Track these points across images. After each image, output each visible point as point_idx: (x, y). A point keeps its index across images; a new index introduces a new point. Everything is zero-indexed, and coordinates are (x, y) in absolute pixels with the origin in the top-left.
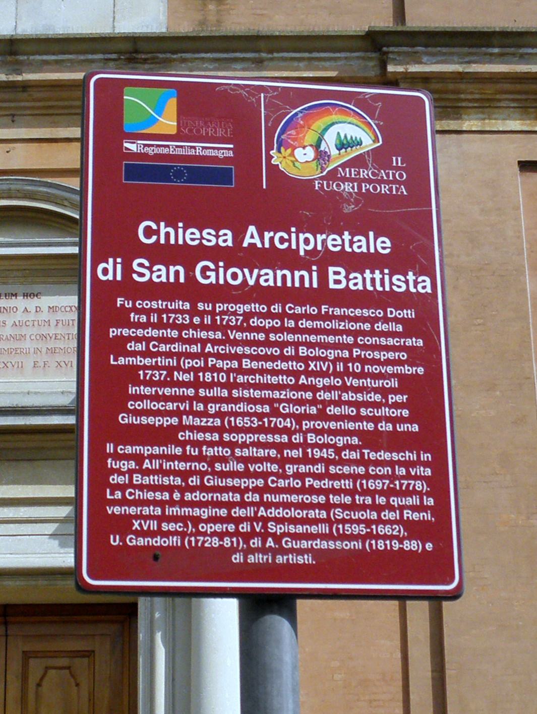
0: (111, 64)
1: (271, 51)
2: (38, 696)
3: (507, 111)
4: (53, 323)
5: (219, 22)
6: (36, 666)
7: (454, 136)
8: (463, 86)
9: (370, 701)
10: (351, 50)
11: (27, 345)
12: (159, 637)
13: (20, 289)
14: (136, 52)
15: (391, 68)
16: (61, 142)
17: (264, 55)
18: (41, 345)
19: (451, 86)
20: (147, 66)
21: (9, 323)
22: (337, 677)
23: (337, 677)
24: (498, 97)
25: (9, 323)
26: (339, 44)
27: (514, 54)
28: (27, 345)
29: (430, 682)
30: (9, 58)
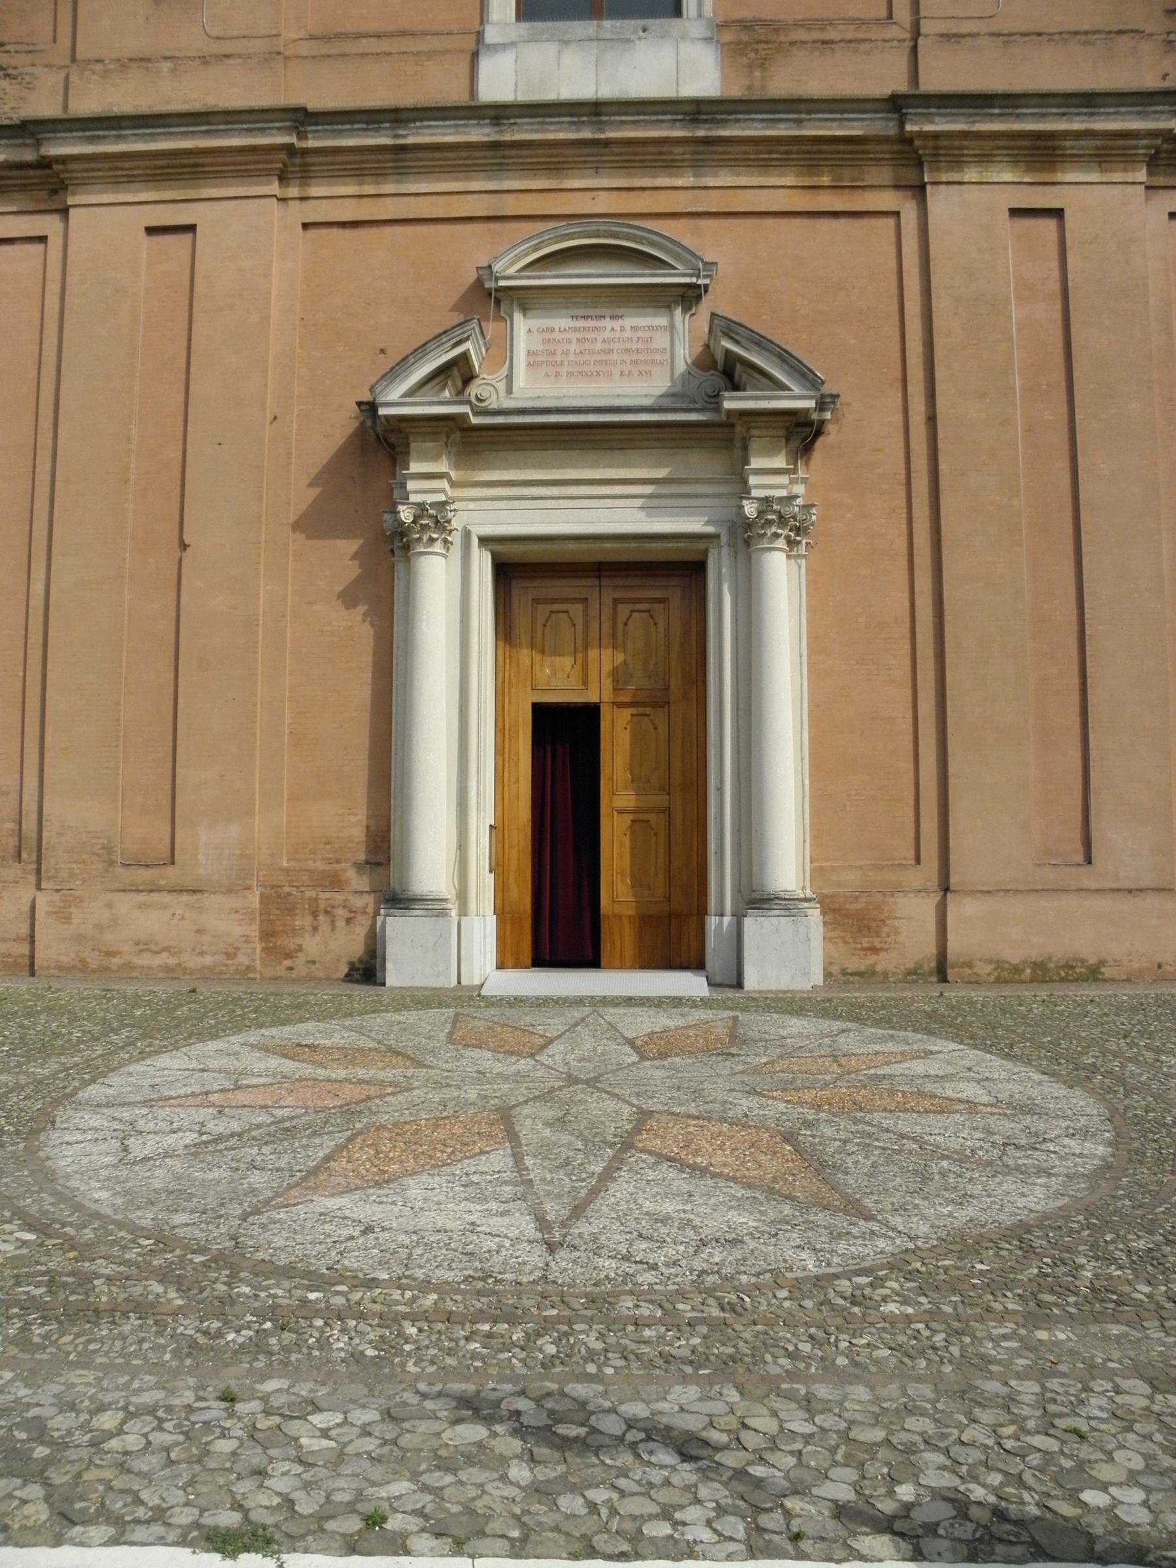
0: (678, 124)
1: (809, 112)
2: (625, 633)
3: (1001, 165)
4: (635, 339)
5: (763, 87)
6: (624, 610)
7: (957, 187)
8: (966, 143)
9: (886, 639)
10: (876, 112)
11: (615, 357)
12: (726, 587)
13: (607, 312)
14: (699, 113)
15: (908, 128)
16: (919, 218)
17: (804, 116)
18: (627, 358)
19: (957, 143)
20: (707, 126)
21: (600, 339)
22: (860, 620)
23: (860, 620)
24: (995, 152)
25: (600, 339)
26: (868, 106)
27: (1010, 115)
28: (615, 357)
29: (931, 625)
30: (594, 119)
